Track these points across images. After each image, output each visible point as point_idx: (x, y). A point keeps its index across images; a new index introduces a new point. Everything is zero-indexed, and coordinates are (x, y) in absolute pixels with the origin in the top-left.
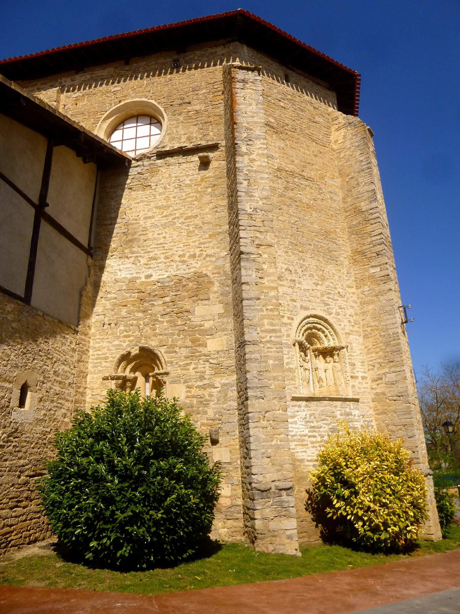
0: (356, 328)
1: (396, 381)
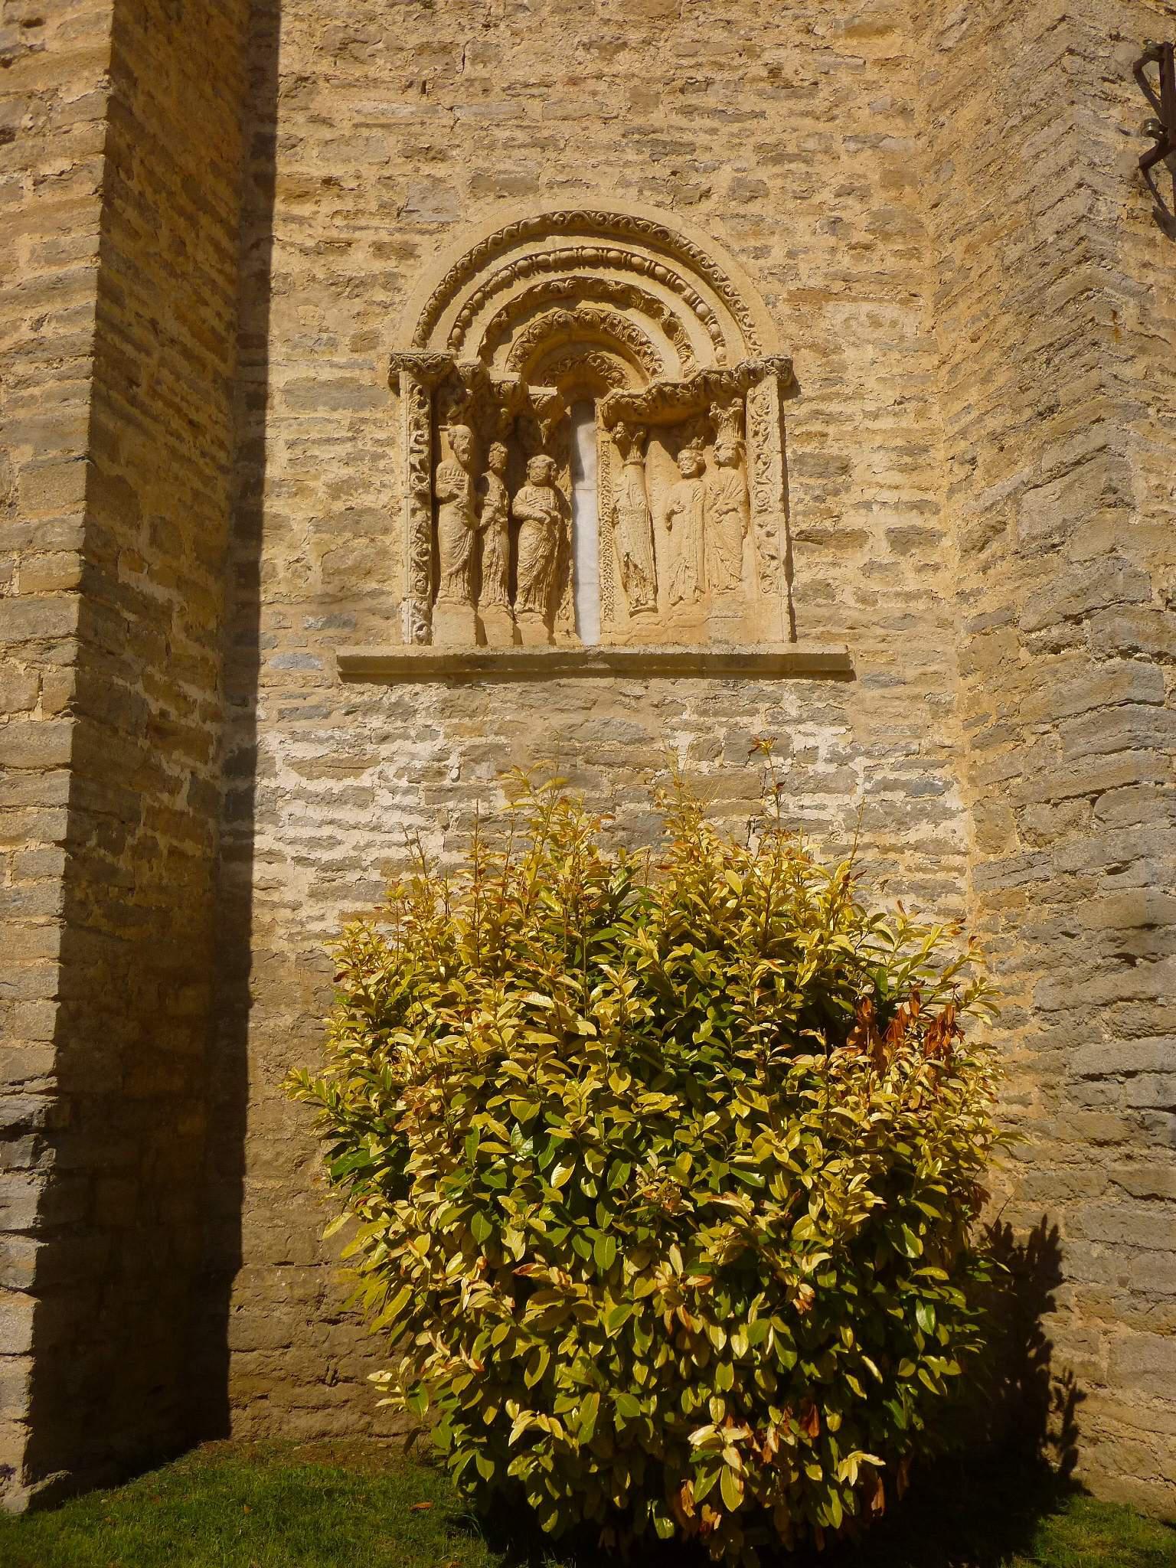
0: (887, 258)
1: (1063, 528)
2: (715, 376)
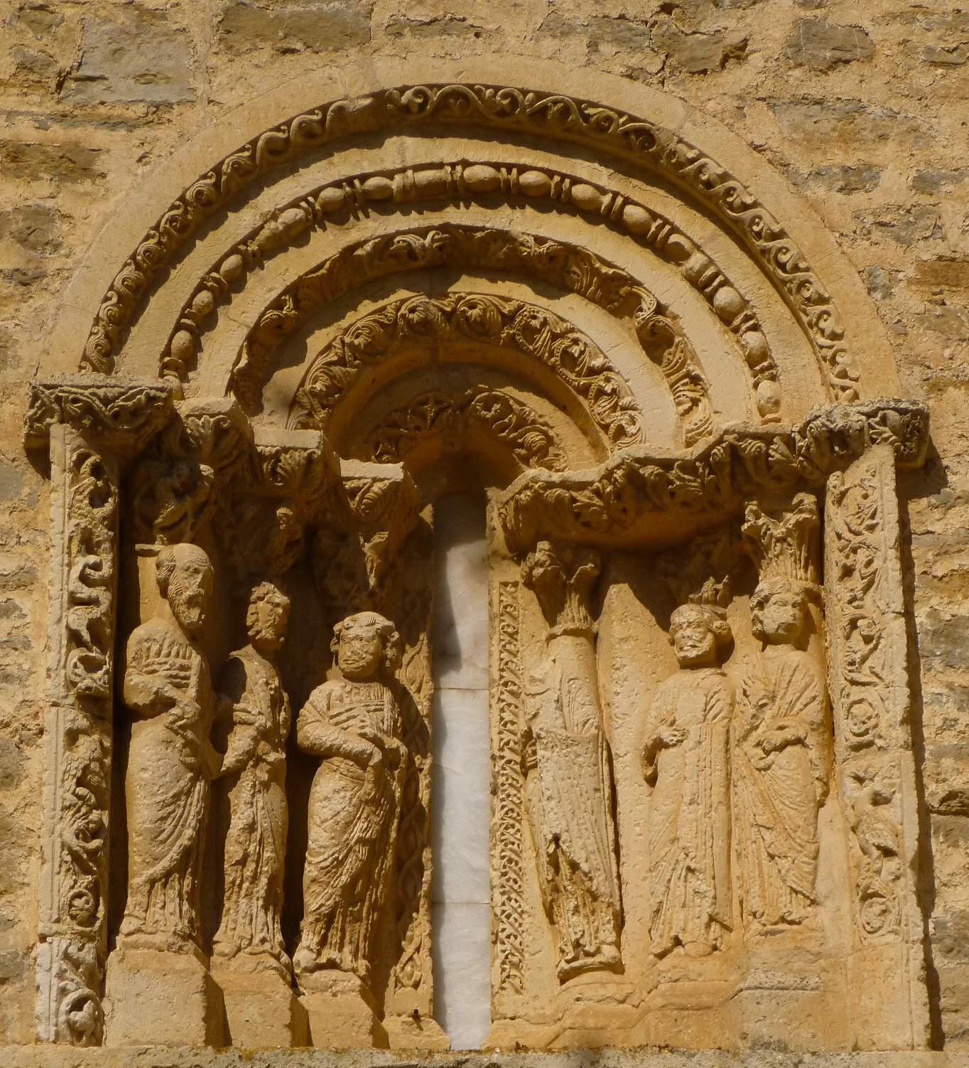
2: (752, 446)
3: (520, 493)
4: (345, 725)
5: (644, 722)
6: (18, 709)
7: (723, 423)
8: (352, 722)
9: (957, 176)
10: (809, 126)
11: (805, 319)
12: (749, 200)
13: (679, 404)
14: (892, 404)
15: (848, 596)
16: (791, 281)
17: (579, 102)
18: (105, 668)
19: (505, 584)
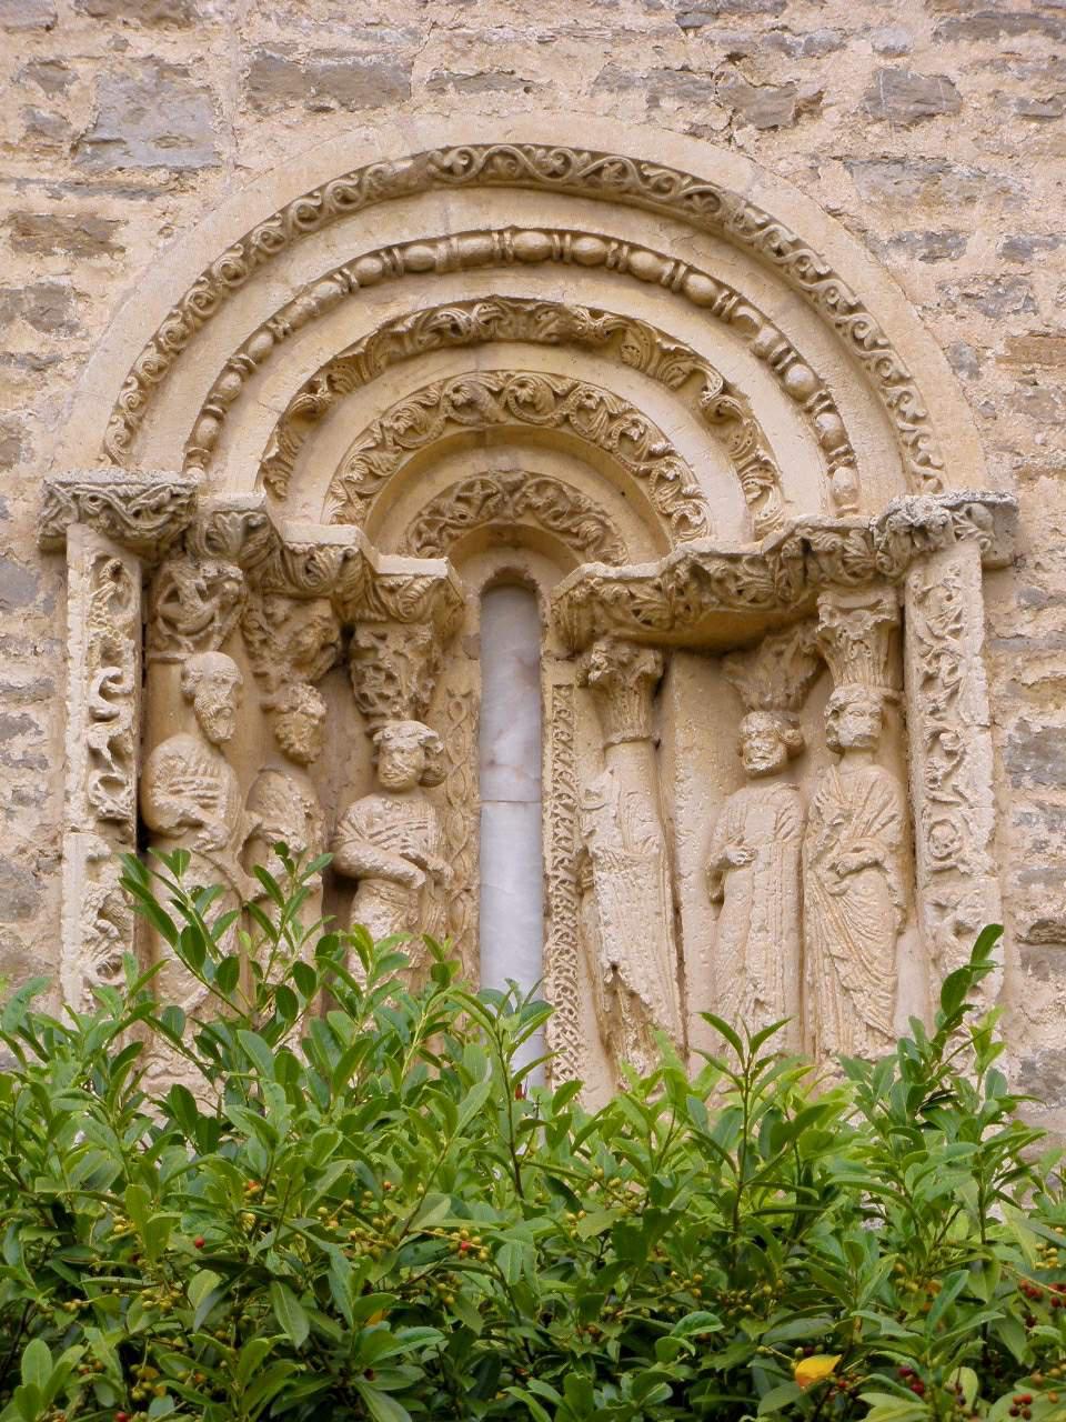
3: (574, 588)
4: (385, 845)
5: (710, 840)
6: (34, 833)
7: (796, 516)
8: (394, 841)
9: (1053, 243)
10: (890, 187)
11: (885, 401)
12: (823, 270)
13: (748, 492)
14: (978, 496)
15: (930, 708)
16: (869, 358)
17: (638, 163)
18: (127, 789)
19: (558, 687)
